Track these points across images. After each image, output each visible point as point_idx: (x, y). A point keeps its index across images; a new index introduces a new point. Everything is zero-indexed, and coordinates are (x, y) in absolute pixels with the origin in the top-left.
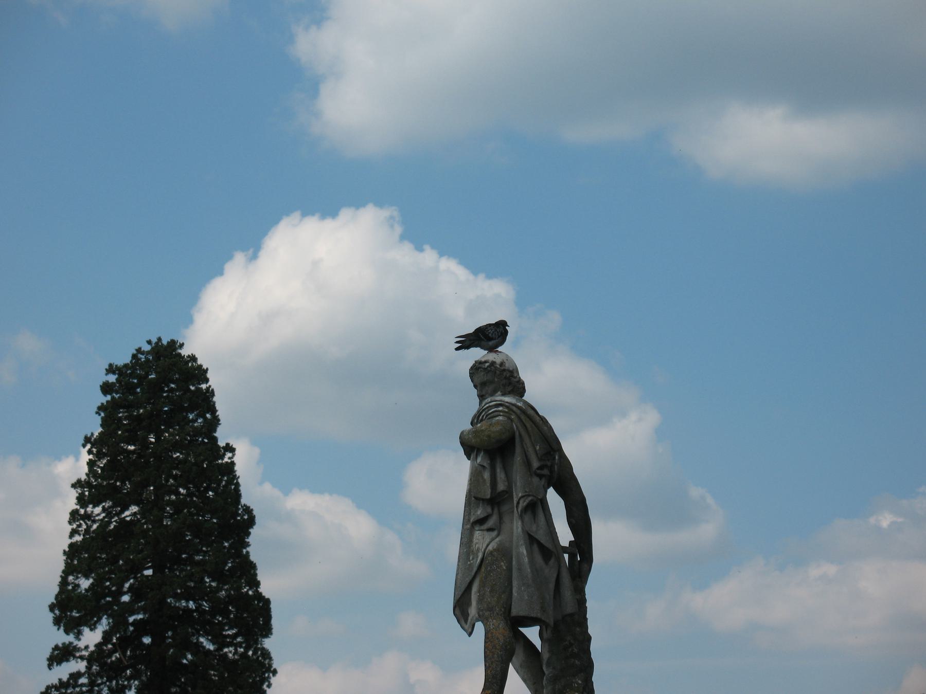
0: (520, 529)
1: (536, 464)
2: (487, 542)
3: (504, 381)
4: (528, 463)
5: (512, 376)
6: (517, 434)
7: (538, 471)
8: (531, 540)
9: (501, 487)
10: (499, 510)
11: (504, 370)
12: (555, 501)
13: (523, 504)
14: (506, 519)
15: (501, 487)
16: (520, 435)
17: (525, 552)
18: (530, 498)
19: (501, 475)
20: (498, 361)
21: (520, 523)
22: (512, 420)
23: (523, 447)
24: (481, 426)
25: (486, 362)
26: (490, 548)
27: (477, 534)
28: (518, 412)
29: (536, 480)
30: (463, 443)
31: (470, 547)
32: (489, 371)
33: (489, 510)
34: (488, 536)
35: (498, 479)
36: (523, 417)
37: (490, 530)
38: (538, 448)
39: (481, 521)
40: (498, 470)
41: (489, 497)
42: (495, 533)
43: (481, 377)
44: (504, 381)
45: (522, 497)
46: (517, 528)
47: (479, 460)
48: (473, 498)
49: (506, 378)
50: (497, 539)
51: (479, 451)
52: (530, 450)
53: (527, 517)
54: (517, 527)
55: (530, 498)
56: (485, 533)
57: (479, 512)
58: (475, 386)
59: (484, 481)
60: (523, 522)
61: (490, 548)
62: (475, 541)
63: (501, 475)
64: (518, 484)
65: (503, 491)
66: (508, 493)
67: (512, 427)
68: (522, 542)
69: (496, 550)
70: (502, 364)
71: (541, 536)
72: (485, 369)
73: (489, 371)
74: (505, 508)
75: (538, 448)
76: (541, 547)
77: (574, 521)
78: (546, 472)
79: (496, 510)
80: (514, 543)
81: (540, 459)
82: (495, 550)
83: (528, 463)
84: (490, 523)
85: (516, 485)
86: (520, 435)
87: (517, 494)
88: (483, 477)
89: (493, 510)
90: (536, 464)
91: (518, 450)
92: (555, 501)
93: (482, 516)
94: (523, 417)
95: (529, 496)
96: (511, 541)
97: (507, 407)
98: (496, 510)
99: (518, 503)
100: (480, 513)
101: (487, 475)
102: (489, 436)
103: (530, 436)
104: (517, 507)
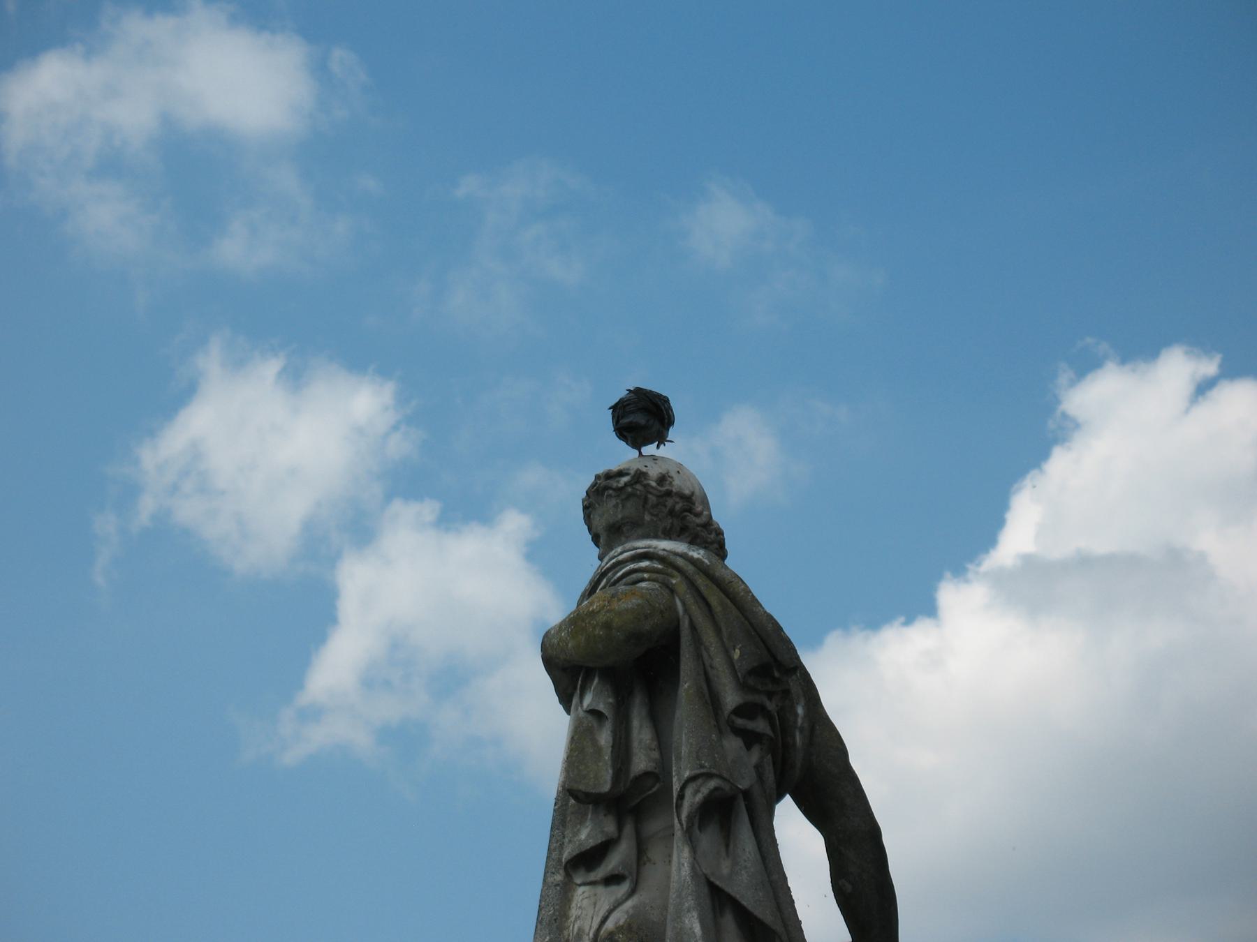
0: (686, 871)
1: (731, 698)
2: (602, 913)
3: (668, 522)
4: (712, 700)
5: (690, 510)
6: (685, 624)
7: (740, 722)
8: (718, 898)
9: (641, 762)
10: (638, 833)
11: (669, 494)
12: (799, 840)
13: (692, 799)
14: (655, 853)
15: (641, 762)
16: (693, 627)
17: (697, 929)
18: (712, 784)
19: (641, 734)
20: (654, 471)
21: (686, 853)
22: (672, 591)
23: (699, 657)
24: (591, 604)
25: (621, 474)
26: (610, 925)
27: (581, 895)
28: (690, 569)
29: (733, 744)
30: (551, 663)
31: (561, 929)
32: (629, 496)
33: (610, 827)
34: (607, 896)
35: (635, 744)
36: (701, 581)
37: (612, 880)
38: (736, 654)
39: (587, 859)
40: (636, 723)
41: (606, 788)
42: (625, 887)
43: (610, 511)
44: (668, 522)
45: (692, 779)
46: (680, 865)
47: (588, 700)
48: (576, 798)
49: (672, 513)
50: (629, 903)
51: (589, 673)
52: (718, 661)
53: (708, 839)
54: (677, 866)
55: (712, 784)
56: (600, 889)
57: (583, 836)
58: (596, 539)
59: (598, 750)
60: (694, 850)
61: (610, 925)
62: (574, 912)
63: (641, 734)
64: (684, 750)
65: (647, 774)
66: (659, 775)
67: (672, 607)
68: (689, 902)
69: (627, 928)
70: (662, 479)
71: (744, 888)
72: (620, 490)
73: (629, 496)
74: (653, 826)
75: (736, 654)
76: (745, 917)
77: (849, 888)
78: (760, 725)
79: (629, 829)
80: (671, 909)
81: (743, 686)
82: (620, 929)
83: (712, 700)
84: (613, 863)
85: (679, 758)
86: (693, 627)
87: (681, 771)
88: (595, 742)
89: (620, 828)
90: (731, 698)
91: (687, 665)
92: (799, 840)
93: (592, 843)
94: (701, 581)
95: (709, 776)
96: (665, 908)
97: (662, 559)
98: (629, 829)
99: (681, 797)
100: (585, 835)
101: (605, 737)
102: (607, 626)
103: (718, 631)
104: (679, 807)
